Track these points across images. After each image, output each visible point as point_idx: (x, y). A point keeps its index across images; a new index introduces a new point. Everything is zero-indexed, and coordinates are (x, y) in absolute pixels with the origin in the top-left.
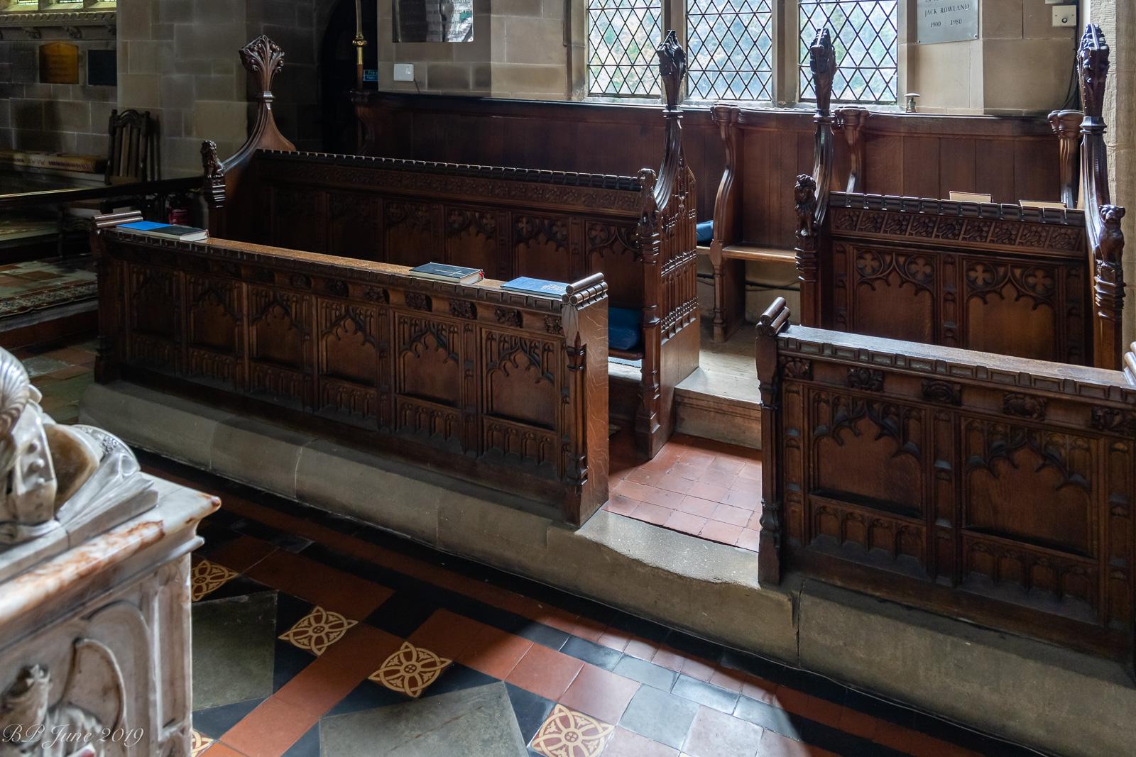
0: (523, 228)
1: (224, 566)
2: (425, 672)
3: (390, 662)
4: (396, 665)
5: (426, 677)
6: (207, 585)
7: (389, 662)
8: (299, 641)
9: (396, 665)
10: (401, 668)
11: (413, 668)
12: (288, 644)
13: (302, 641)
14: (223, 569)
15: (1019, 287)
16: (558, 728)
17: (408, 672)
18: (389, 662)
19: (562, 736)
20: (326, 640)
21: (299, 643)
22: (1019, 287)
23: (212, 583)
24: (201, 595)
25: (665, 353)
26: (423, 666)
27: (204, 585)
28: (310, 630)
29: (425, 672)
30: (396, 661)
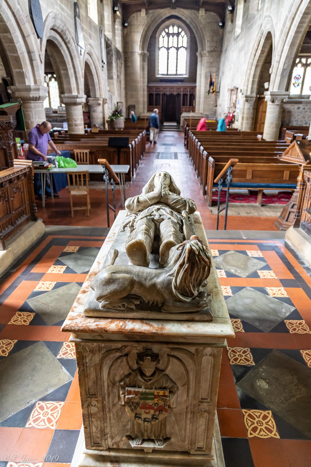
0: (62, 127)
1: (302, 357)
2: (256, 416)
3: (264, 435)
4: (54, 413)
5: (55, 415)
6: (298, 330)
7: (33, 415)
8: (272, 426)
9: (37, 415)
10: (50, 413)
11: (241, 356)
12: (255, 360)
13: (270, 425)
14: (304, 358)
15: (205, 276)
16: (53, 416)
17: (46, 412)
18: (33, 415)
19: (257, 419)
20: (6, 350)
21: (273, 425)
22: (205, 276)
23: (243, 360)
24: (274, 296)
25: (73, 131)
26: (266, 428)
27: (297, 329)
28: (300, 328)
29: (264, 431)
30: (262, 433)
